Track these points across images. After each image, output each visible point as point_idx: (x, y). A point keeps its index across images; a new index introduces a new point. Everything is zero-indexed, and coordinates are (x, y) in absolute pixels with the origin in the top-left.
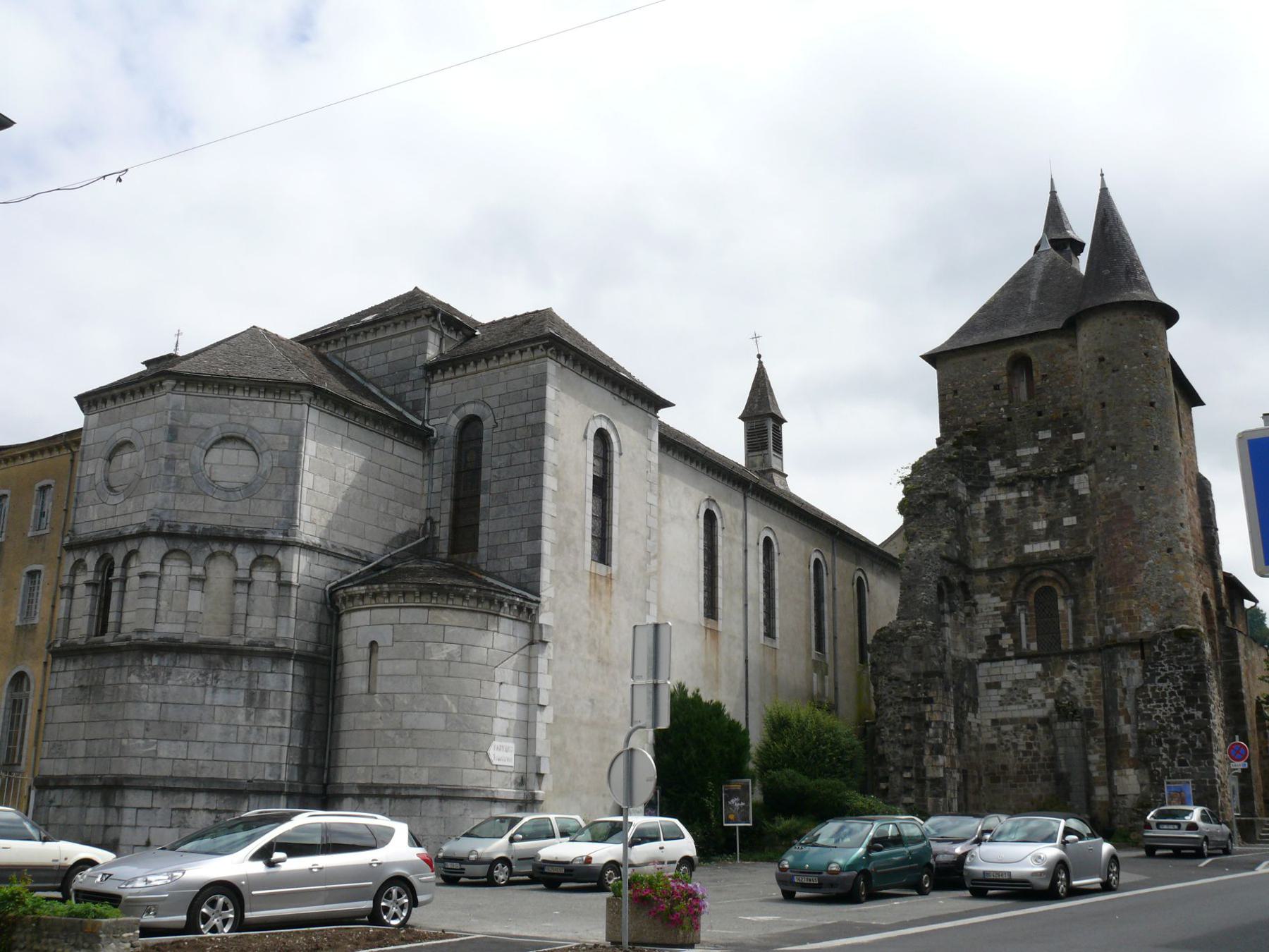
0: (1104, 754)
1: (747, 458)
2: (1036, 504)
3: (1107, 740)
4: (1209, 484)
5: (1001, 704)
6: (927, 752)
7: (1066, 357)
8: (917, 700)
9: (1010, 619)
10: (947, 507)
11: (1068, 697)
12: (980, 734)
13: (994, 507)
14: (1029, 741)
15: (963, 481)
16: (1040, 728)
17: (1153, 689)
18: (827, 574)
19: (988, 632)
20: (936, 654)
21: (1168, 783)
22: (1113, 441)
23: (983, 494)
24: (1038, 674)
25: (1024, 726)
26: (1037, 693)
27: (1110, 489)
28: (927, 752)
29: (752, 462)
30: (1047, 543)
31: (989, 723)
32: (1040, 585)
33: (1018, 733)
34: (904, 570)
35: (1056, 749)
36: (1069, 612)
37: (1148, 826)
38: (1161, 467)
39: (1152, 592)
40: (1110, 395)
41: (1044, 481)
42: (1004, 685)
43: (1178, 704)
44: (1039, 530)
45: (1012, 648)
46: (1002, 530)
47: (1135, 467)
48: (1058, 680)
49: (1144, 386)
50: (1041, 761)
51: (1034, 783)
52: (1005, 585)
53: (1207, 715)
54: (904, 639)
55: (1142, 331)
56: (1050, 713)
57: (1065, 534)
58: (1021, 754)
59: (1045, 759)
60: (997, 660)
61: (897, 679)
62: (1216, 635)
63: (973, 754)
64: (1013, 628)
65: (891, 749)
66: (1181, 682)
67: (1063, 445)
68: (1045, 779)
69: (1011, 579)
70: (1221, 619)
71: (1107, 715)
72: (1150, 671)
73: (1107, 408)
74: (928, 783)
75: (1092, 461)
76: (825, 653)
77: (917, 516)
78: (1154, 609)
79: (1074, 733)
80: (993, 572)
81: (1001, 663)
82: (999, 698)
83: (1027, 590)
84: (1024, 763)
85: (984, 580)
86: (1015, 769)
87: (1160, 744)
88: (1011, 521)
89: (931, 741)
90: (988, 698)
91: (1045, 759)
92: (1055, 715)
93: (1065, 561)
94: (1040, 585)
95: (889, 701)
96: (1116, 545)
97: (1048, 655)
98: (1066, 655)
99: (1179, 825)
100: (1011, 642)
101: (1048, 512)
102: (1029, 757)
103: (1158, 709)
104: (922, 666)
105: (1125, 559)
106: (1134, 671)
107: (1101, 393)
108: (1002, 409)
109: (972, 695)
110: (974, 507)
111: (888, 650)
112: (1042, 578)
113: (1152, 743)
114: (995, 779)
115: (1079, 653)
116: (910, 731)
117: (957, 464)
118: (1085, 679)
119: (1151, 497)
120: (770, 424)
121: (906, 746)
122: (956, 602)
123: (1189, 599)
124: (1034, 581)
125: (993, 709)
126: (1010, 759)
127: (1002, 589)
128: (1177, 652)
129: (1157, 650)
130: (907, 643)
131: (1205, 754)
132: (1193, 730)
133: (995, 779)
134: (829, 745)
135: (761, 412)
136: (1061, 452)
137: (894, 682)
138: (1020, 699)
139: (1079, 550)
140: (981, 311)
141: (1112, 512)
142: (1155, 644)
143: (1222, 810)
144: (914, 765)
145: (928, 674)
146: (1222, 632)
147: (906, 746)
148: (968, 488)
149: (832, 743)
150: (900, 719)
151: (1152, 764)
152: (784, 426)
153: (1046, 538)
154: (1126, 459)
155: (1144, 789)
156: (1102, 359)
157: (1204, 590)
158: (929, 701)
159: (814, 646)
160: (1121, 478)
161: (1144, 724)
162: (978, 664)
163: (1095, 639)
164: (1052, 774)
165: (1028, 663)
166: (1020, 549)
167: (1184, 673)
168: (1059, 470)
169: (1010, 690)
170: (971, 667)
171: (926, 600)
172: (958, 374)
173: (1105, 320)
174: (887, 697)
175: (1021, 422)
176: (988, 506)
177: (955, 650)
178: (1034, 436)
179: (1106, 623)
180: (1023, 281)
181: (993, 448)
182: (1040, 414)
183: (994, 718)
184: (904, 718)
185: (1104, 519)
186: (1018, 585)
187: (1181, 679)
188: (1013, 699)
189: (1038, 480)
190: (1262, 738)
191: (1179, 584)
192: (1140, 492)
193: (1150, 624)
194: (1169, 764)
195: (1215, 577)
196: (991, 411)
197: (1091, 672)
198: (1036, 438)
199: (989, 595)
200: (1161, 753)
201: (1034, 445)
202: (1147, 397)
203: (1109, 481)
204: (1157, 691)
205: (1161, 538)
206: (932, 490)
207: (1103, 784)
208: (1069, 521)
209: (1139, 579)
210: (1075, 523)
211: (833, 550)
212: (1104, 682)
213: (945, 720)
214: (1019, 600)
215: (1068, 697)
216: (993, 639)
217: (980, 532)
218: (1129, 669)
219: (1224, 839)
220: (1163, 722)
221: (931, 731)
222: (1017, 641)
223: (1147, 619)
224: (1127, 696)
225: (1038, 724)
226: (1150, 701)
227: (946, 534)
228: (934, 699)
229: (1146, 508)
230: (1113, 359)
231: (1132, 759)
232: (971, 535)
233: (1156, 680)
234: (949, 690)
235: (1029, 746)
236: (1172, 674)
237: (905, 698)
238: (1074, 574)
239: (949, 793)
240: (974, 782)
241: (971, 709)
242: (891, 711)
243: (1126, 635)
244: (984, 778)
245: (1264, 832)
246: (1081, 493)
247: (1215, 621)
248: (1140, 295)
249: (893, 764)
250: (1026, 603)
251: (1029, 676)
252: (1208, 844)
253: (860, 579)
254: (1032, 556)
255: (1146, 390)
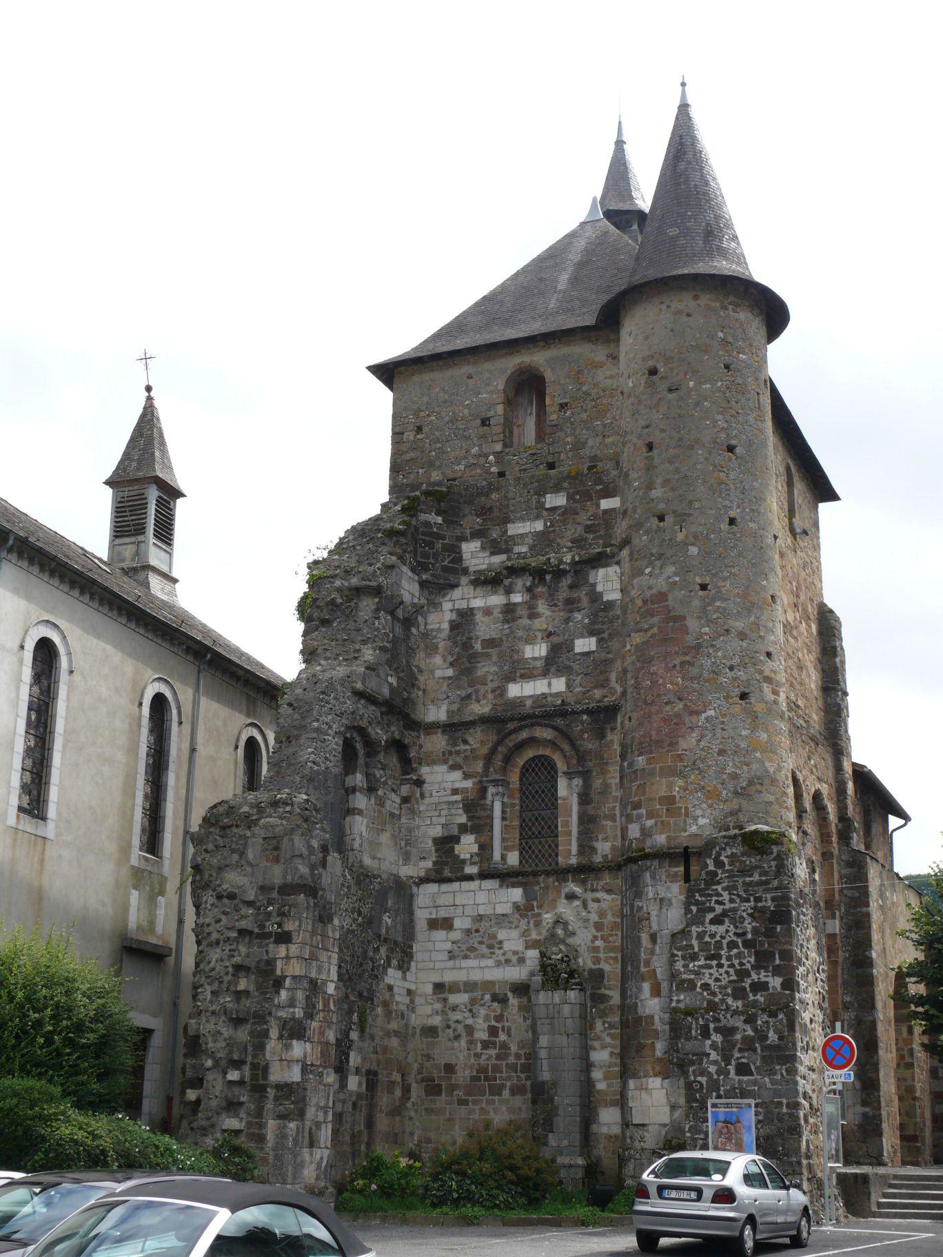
0: (617, 1051)
1: (112, 547)
2: (533, 616)
3: (624, 1024)
4: (837, 620)
5: (452, 956)
6: (274, 1034)
7: (601, 375)
8: (264, 936)
9: (475, 806)
10: (377, 610)
11: (562, 947)
12: (412, 1007)
13: (464, 618)
14: (493, 1023)
15: (413, 570)
16: (513, 1001)
17: (700, 936)
18: (180, 723)
19: (437, 831)
20: (305, 851)
21: (714, 1106)
22: (662, 506)
23: (447, 598)
24: (516, 906)
25: (487, 997)
26: (511, 940)
27: (650, 588)
28: (274, 1034)
29: (119, 554)
30: (545, 682)
31: (429, 989)
32: (530, 753)
33: (475, 1008)
34: (284, 710)
35: (535, 1039)
36: (574, 801)
37: (643, 1192)
38: (740, 554)
39: (709, 766)
40: (662, 431)
41: (548, 577)
42: (458, 923)
43: (741, 964)
44: (534, 659)
45: (476, 859)
46: (473, 658)
47: (694, 550)
48: (548, 917)
49: (720, 417)
50: (512, 1059)
51: (496, 1098)
52: (472, 750)
53: (790, 984)
54: (250, 823)
55: (723, 328)
56: (532, 974)
57: (576, 666)
58: (479, 1045)
59: (517, 1056)
60: (450, 880)
61: (232, 896)
62: (835, 861)
63: (394, 1042)
64: (478, 823)
65: (211, 1027)
66: (748, 925)
67: (583, 518)
68: (517, 1090)
69: (482, 742)
70: (844, 837)
71: (624, 978)
72: (697, 903)
73: (655, 452)
74: (271, 1093)
75: (626, 542)
76: (161, 858)
77: (325, 622)
78: (712, 795)
79: (566, 1009)
80: (454, 728)
81: (456, 885)
82: (448, 946)
83: (507, 759)
84: (482, 1061)
85: (438, 742)
86: (467, 1072)
87: (706, 1034)
88: (490, 643)
89: (282, 1014)
90: (431, 947)
91: (517, 1056)
92: (538, 979)
93: (573, 713)
94: (530, 753)
95: (215, 936)
96: (654, 683)
97: (535, 874)
98: (563, 873)
99: (699, 1191)
100: (475, 848)
101: (551, 629)
102: (493, 1052)
103: (707, 971)
104: (276, 874)
105: (668, 708)
106: (670, 904)
107: (647, 427)
108: (491, 457)
109: (400, 939)
110: (432, 618)
111: (221, 841)
112: (532, 741)
113: (693, 1032)
114: (433, 1089)
115: (585, 871)
116: (246, 993)
117: (403, 540)
118: (594, 917)
119: (718, 604)
120: (153, 494)
121: (237, 1022)
122: (378, 773)
123: (774, 781)
124: (521, 746)
125: (438, 966)
126: (460, 1054)
127: (466, 758)
128: (745, 872)
129: (711, 867)
130: (256, 830)
131: (783, 1055)
132: (763, 1010)
133: (433, 1089)
134: (49, 1011)
135: (141, 474)
136: (580, 529)
137: (225, 901)
138: (483, 949)
139: (597, 693)
140: (477, 305)
141: (651, 627)
142: (710, 857)
143: (808, 1157)
144: (249, 1059)
145: (287, 889)
146: (844, 857)
147: (237, 1022)
148: (423, 585)
149: (57, 1006)
150: (230, 970)
151: (691, 1069)
152: (180, 502)
153: (545, 673)
154: (680, 537)
155: (677, 1114)
156: (653, 372)
157: (818, 786)
158: (284, 938)
159: (136, 841)
160: (671, 569)
161: (682, 997)
162: (418, 885)
163: (613, 848)
164: (529, 1083)
165: (501, 886)
166: (500, 691)
167: (754, 908)
168: (573, 557)
169: (468, 932)
170: (402, 891)
171: (314, 763)
172: (425, 399)
173: (664, 307)
174: (211, 929)
175: (519, 479)
176: (454, 616)
177: (374, 858)
178: (538, 502)
179: (629, 819)
180: (551, 262)
181: (471, 521)
182: (551, 466)
183: (438, 980)
184: (238, 968)
185: (637, 638)
186: (493, 751)
187: (749, 920)
188: (472, 949)
189: (539, 574)
190: (905, 1034)
191: (758, 755)
192: (701, 593)
193: (702, 821)
194: (719, 1072)
195: (839, 769)
196: (473, 461)
197: (604, 905)
198: (541, 506)
199: (445, 767)
200: (708, 1050)
201: (537, 517)
202: (723, 435)
203: (650, 575)
204: (707, 939)
205: (730, 674)
206: (355, 581)
207: (613, 1104)
208: (584, 645)
209: (688, 742)
210: (594, 648)
211: (198, 680)
212: (622, 922)
213: (313, 975)
214: (494, 776)
215: (562, 947)
216: (446, 844)
217: (438, 660)
218: (661, 900)
219: (791, 1219)
220: (714, 994)
221: (284, 994)
222: (485, 848)
223: (699, 812)
224: (657, 948)
225: (510, 995)
226: (694, 957)
227: (369, 654)
228: (294, 935)
229: (709, 622)
230: (672, 369)
231: (660, 1060)
232: (422, 665)
233: (707, 921)
234: (330, 920)
235: (493, 1031)
236: (735, 910)
237: (243, 932)
238: (586, 735)
239: (311, 1112)
240: (390, 1092)
241: (394, 962)
242: (218, 956)
243: (661, 839)
244: (414, 1085)
245: (885, 1196)
246: (607, 597)
247: (834, 839)
248: (723, 266)
249: (212, 1055)
250: (505, 783)
251: (500, 910)
252: (754, 1229)
253: (251, 742)
254: (520, 701)
255: (722, 424)
